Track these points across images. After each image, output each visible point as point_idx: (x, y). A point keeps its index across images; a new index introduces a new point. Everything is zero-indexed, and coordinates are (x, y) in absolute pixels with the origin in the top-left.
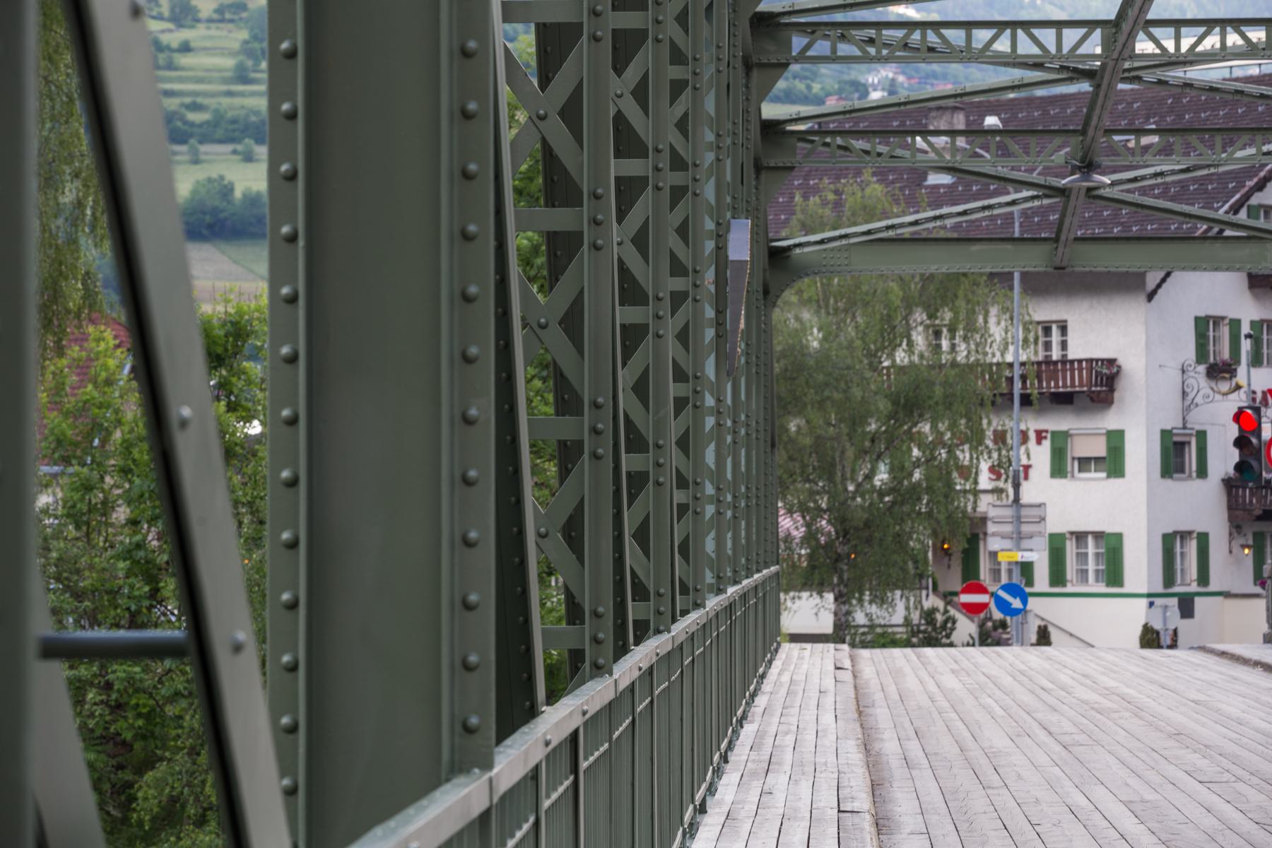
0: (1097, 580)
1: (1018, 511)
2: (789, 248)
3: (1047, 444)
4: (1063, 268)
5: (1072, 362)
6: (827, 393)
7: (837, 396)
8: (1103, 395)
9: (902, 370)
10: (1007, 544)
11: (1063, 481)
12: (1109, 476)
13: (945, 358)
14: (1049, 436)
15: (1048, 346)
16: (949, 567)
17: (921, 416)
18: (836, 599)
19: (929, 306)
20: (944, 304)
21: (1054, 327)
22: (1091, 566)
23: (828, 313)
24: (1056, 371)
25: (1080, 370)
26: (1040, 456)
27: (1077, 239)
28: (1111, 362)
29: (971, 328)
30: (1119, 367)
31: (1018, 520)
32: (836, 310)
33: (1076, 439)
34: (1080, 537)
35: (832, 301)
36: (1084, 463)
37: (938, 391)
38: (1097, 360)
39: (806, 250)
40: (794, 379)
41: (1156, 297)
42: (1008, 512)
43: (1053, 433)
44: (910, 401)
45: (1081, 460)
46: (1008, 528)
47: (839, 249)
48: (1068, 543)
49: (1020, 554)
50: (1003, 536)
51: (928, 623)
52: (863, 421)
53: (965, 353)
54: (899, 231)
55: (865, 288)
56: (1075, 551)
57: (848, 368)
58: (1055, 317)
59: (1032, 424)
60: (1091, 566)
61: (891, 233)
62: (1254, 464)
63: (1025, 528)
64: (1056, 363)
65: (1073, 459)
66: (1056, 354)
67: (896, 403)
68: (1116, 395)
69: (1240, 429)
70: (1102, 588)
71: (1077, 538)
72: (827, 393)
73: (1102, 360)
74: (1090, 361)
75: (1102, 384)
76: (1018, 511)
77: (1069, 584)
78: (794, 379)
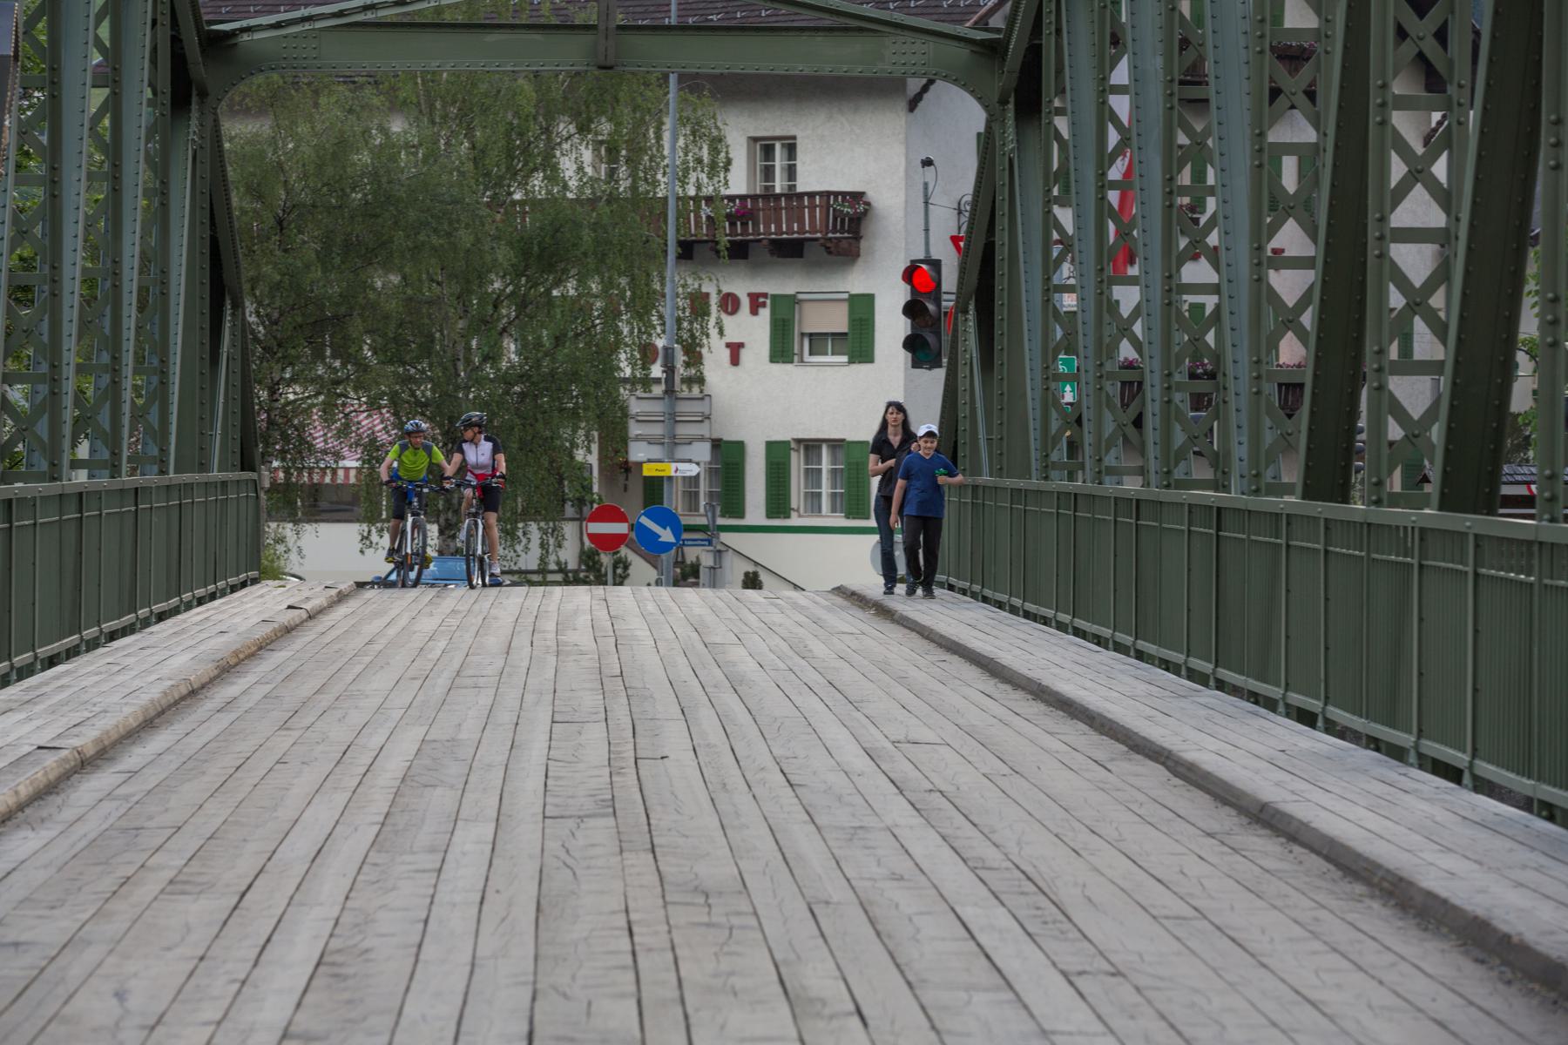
0: (834, 510)
1: (672, 406)
2: (233, 34)
3: (765, 313)
4: (611, 68)
5: (802, 195)
6: (422, 237)
7: (435, 241)
8: (844, 244)
9: (535, 204)
10: (656, 452)
11: (788, 366)
12: (851, 362)
13: (779, 186)
14: (768, 302)
15: (768, 173)
16: (626, 489)
17: (565, 271)
18: (441, 532)
19: (580, 114)
20: (600, 113)
21: (778, 146)
22: (825, 489)
23: (433, 123)
24: (778, 209)
25: (812, 208)
26: (754, 329)
27: (620, 28)
28: (857, 196)
29: (637, 150)
30: (868, 204)
31: (673, 418)
32: (445, 117)
33: (806, 306)
34: (811, 447)
35: (438, 105)
36: (818, 342)
37: (587, 235)
38: (836, 194)
39: (257, 36)
40: (376, 216)
41: (921, 105)
42: (657, 407)
43: (774, 297)
44: (548, 249)
45: (811, 336)
46: (657, 430)
47: (304, 36)
48: (794, 455)
49: (673, 466)
50: (651, 441)
51: (589, 569)
52: (482, 279)
53: (628, 183)
54: (381, 13)
55: (483, 87)
56: (803, 466)
57: (455, 202)
58: (778, 133)
59: (741, 286)
60: (825, 489)
61: (369, 16)
62: (930, 338)
63: (683, 430)
64: (778, 197)
65: (803, 335)
66: (779, 186)
67: (525, 253)
68: (863, 244)
69: (914, 291)
70: (841, 521)
71: (807, 448)
72: (422, 237)
73: (844, 194)
74: (828, 194)
75: (843, 227)
76: (672, 406)
77: (794, 514)
78: (376, 216)
